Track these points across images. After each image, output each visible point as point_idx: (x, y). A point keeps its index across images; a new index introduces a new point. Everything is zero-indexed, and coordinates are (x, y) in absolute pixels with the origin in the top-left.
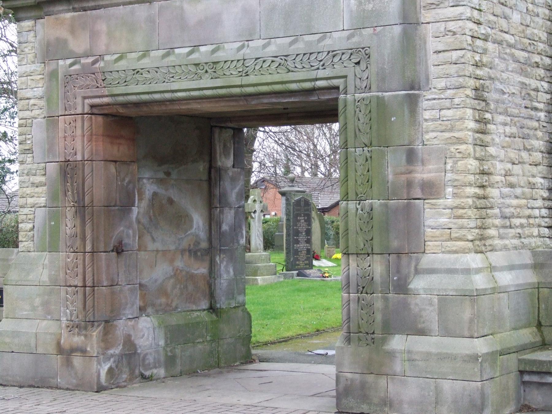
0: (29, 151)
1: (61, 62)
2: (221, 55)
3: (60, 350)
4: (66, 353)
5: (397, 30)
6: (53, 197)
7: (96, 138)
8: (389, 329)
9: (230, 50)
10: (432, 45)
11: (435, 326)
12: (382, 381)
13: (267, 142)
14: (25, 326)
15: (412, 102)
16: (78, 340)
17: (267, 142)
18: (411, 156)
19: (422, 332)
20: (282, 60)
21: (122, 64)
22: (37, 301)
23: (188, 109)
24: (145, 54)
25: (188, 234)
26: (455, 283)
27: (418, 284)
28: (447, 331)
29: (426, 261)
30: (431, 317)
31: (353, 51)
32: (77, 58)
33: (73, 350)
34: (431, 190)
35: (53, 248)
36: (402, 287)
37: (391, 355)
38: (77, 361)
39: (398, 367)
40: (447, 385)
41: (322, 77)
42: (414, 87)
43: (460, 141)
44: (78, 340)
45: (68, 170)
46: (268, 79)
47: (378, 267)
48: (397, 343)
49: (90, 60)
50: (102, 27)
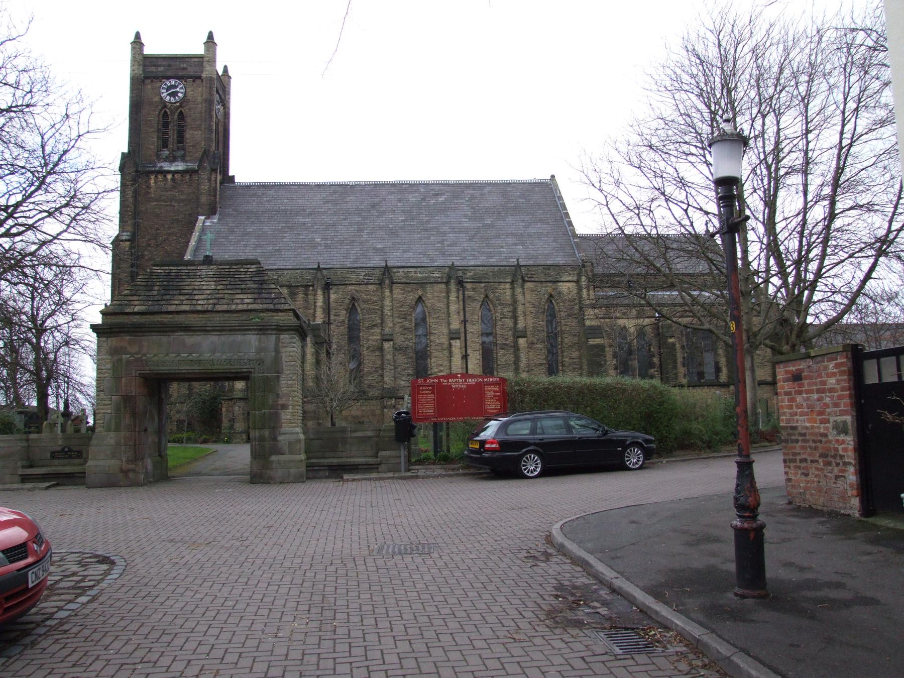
0: (102, 391)
1: (124, 356)
2: (201, 358)
3: (122, 471)
4: (125, 472)
5: (273, 354)
6: (118, 409)
7: (845, 422)
8: (271, 454)
9: (207, 356)
10: (284, 359)
11: (287, 452)
12: (268, 471)
13: (174, 388)
14: (102, 463)
15: (278, 377)
16: (131, 466)
17: (174, 388)
18: (278, 396)
19: (282, 454)
20: (229, 361)
21: (156, 358)
22: (108, 452)
23: (595, 385)
24: (167, 355)
25: (871, 520)
26: (294, 437)
27: (280, 438)
28: (291, 453)
29: (283, 430)
30: (286, 448)
31: (257, 360)
32: (132, 355)
33: (128, 471)
34: (284, 407)
35: (117, 429)
36: (275, 439)
37: (272, 462)
38: (131, 475)
39: (274, 466)
40: (292, 470)
41: (245, 368)
42: (279, 372)
43: (294, 391)
44: (131, 466)
45: (127, 399)
46: (174, 368)
47: (266, 433)
48: (274, 458)
49: (139, 356)
50: (146, 344)
